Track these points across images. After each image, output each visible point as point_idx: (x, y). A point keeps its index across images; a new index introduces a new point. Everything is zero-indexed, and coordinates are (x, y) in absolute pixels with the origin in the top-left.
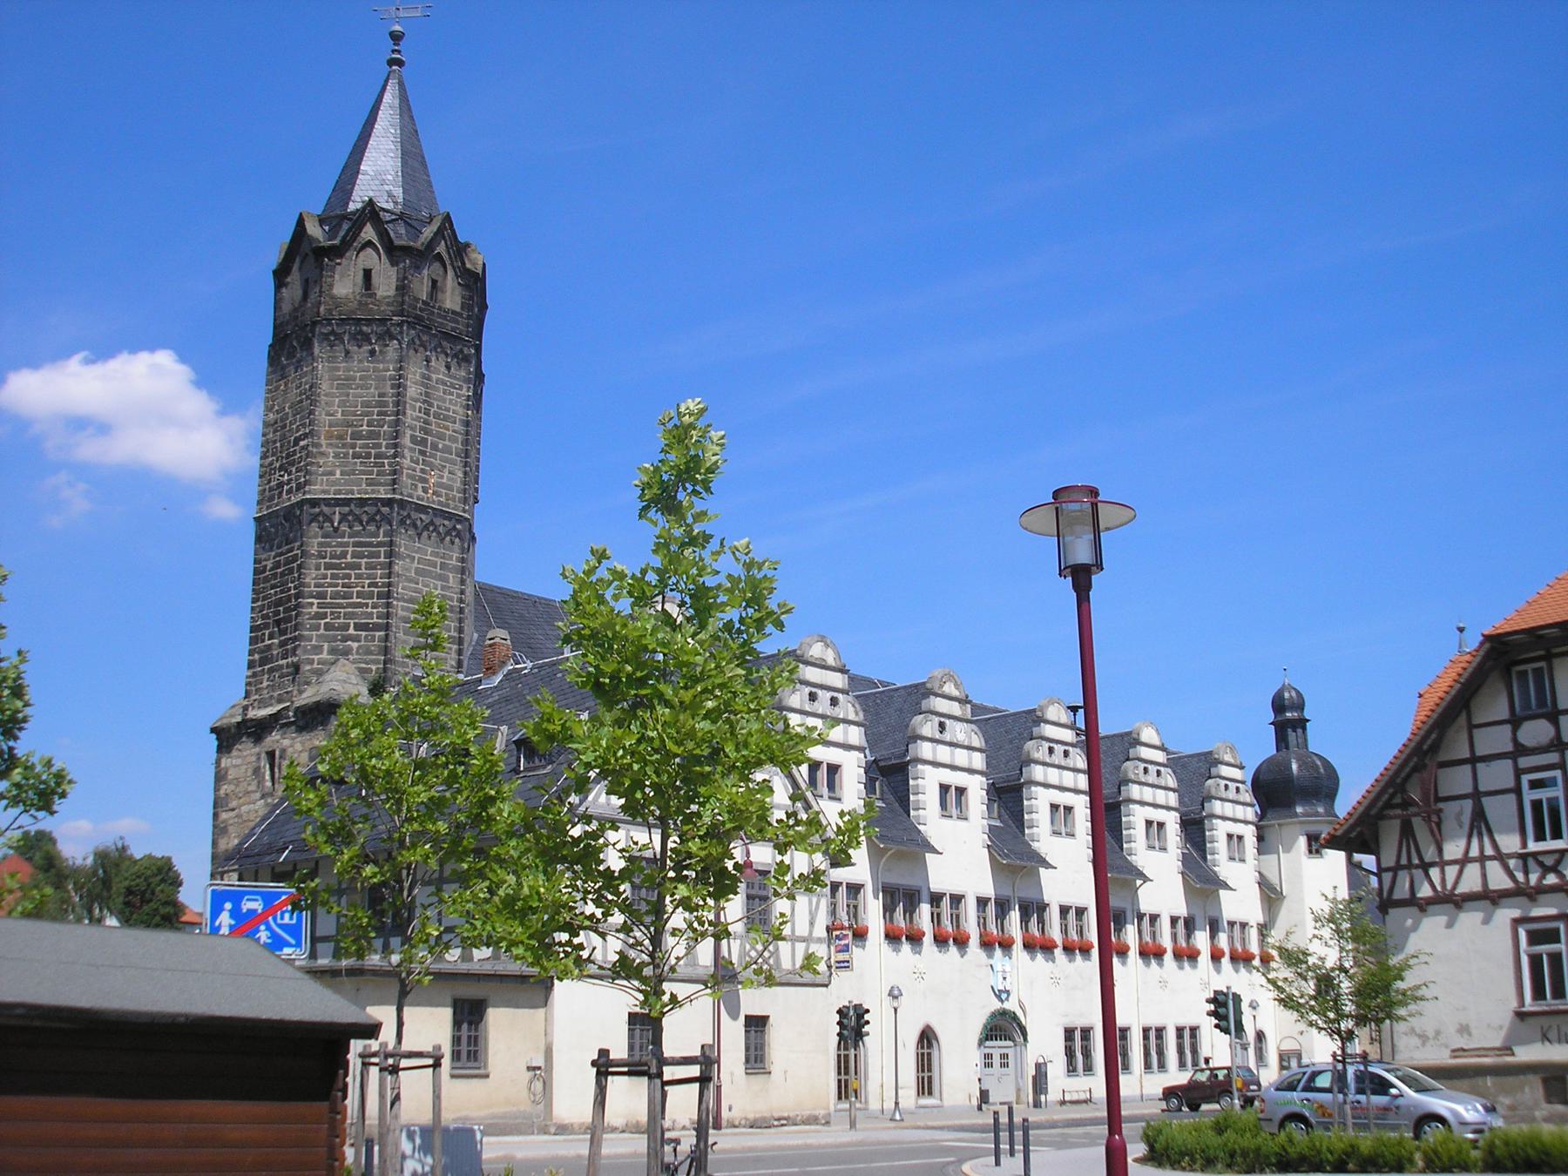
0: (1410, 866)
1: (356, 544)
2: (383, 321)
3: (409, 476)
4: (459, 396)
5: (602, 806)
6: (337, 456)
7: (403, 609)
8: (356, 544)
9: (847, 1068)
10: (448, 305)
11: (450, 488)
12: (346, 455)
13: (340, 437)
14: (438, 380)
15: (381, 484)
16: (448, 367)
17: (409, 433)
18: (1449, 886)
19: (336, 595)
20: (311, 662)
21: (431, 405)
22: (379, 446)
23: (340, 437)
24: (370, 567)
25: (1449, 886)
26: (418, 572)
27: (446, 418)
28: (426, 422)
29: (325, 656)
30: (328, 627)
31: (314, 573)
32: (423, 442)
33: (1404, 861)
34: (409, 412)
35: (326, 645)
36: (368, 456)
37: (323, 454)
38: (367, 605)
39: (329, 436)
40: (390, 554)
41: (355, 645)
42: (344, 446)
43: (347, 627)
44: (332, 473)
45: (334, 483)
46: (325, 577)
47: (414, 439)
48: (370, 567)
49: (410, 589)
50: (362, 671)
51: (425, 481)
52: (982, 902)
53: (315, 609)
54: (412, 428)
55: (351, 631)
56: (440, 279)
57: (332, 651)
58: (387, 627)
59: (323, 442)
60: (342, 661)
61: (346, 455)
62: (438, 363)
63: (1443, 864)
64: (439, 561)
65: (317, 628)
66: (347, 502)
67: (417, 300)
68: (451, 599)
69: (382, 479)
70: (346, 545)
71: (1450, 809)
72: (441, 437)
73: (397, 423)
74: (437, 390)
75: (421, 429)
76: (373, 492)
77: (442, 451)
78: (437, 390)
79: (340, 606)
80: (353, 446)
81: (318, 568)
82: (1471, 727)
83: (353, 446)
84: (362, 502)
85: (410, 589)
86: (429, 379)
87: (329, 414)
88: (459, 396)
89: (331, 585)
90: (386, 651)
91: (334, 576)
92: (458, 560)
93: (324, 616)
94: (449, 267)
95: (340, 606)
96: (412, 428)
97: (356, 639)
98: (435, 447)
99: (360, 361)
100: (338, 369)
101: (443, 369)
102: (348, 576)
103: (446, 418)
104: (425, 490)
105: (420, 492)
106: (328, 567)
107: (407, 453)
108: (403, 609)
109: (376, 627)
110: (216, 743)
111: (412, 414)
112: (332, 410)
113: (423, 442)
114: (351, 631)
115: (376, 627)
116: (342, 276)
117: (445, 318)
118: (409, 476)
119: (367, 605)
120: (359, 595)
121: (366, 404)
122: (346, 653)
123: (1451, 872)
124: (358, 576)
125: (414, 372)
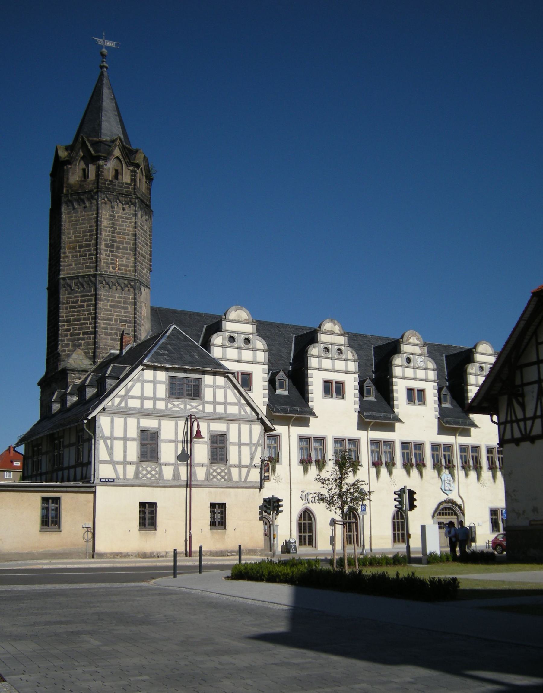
0: (512, 422)
1: (82, 296)
2: (89, 192)
3: (104, 263)
4: (130, 223)
5: (123, 408)
6: (73, 257)
7: (104, 323)
8: (82, 296)
9: (398, 528)
10: (125, 180)
11: (128, 266)
12: (77, 256)
13: (74, 248)
14: (118, 217)
15: (91, 268)
16: (124, 209)
17: (104, 243)
18: (528, 432)
19: (74, 320)
20: (65, 351)
21: (116, 229)
22: (90, 250)
23: (74, 248)
24: (88, 306)
25: (528, 432)
26: (111, 306)
27: (124, 234)
28: (113, 237)
29: (70, 348)
30: (72, 335)
31: (65, 311)
32: (112, 246)
33: (509, 419)
34: (103, 233)
35: (71, 343)
36: (86, 255)
37: (67, 257)
38: (87, 323)
39: (70, 248)
40: (96, 300)
41: (83, 342)
42: (76, 252)
43: (79, 334)
44: (71, 265)
45: (73, 269)
46: (69, 312)
47: (107, 245)
48: (88, 306)
49: (108, 315)
50: (85, 353)
51: (114, 264)
52: (490, 450)
53: (66, 327)
54: (105, 240)
55: (81, 336)
56: (119, 169)
57: (74, 345)
58: (95, 333)
59: (67, 251)
60: (78, 349)
61: (77, 256)
62: (118, 207)
63: (525, 419)
64: (122, 300)
65: (67, 335)
66: (77, 277)
67: (106, 180)
68: (130, 317)
69: (92, 265)
70: (77, 297)
71: (527, 389)
72: (122, 243)
73: (97, 239)
74: (119, 221)
75: (110, 240)
76: (89, 271)
77: (122, 249)
78: (119, 221)
79: (76, 325)
80: (80, 252)
81: (66, 309)
82: (538, 344)
83: (80, 252)
84: (83, 277)
85: (108, 315)
86: (114, 216)
87: (68, 238)
88: (130, 223)
89: (72, 316)
90: (95, 343)
91: (73, 312)
92: (132, 299)
93: (69, 330)
94: (123, 163)
95: (76, 325)
96: (105, 240)
97: (83, 339)
98: (118, 248)
99: (81, 212)
100: (72, 217)
101: (121, 211)
102: (79, 311)
103: (124, 234)
104: (114, 268)
105: (111, 269)
106: (71, 307)
107: (103, 252)
108: (104, 323)
109: (91, 333)
110: (40, 390)
111: (105, 235)
112: (70, 236)
113: (112, 246)
114: (81, 336)
115: (91, 333)
116: (73, 174)
117: (122, 187)
118: (104, 263)
119: (87, 323)
120: (84, 319)
121: (84, 232)
122: (79, 345)
123: (529, 423)
124: (84, 311)
125: (105, 214)
